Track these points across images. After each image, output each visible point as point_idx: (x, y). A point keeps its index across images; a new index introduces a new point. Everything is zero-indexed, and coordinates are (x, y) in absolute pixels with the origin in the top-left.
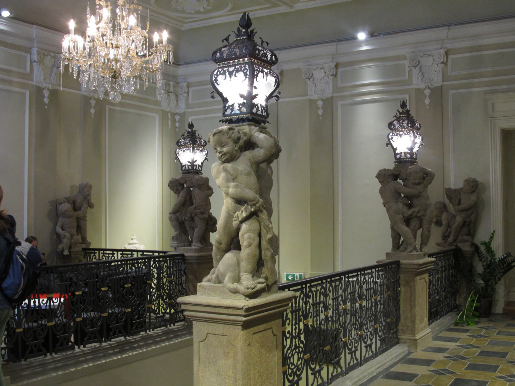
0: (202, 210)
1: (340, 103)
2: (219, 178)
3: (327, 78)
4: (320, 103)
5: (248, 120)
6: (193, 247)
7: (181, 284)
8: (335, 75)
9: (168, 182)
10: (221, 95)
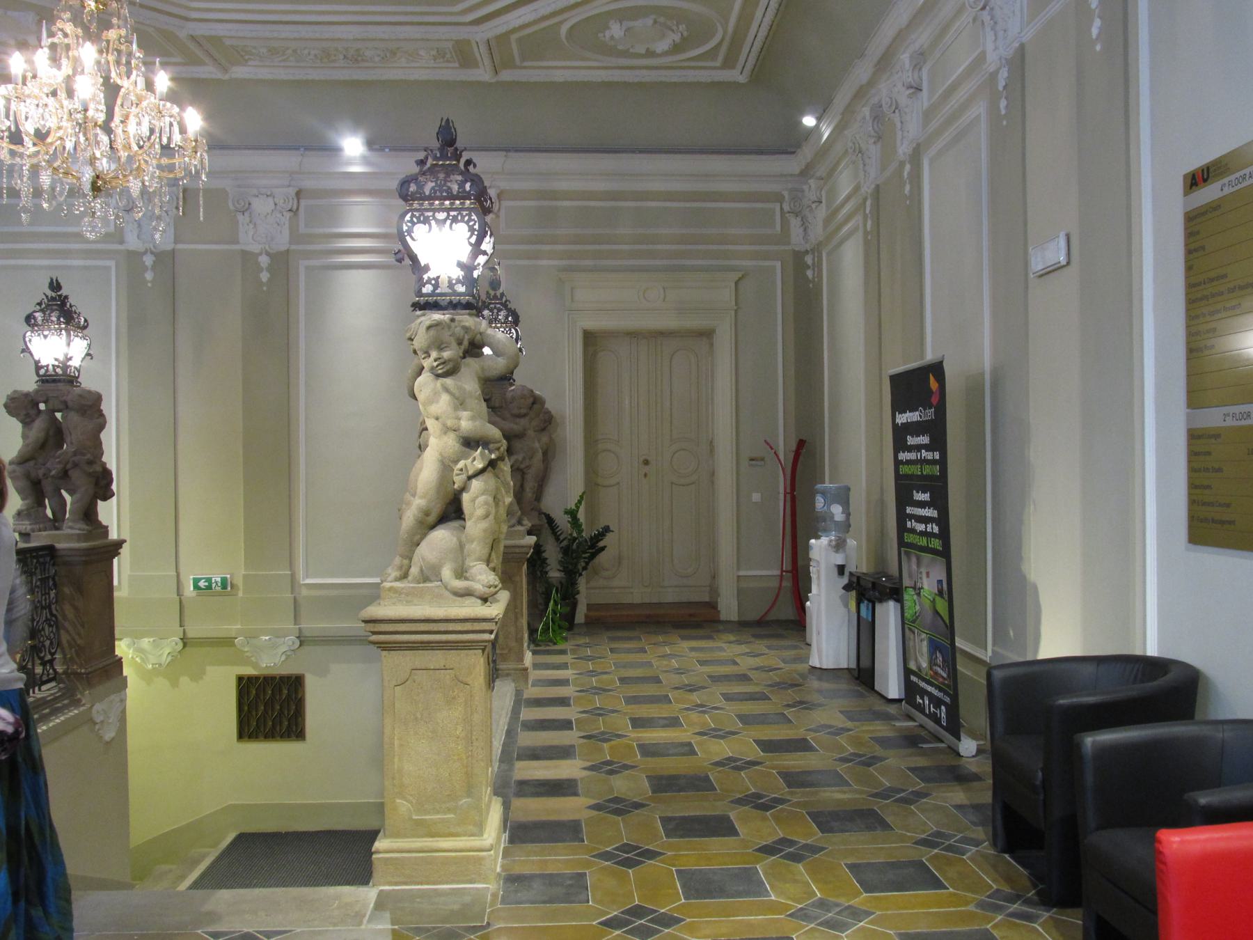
0: (88, 456)
1: (303, 264)
2: (437, 402)
3: (279, 215)
4: (264, 260)
5: (468, 306)
6: (66, 531)
7: (49, 607)
8: (294, 212)
9: (553, 412)
10: (414, 258)
